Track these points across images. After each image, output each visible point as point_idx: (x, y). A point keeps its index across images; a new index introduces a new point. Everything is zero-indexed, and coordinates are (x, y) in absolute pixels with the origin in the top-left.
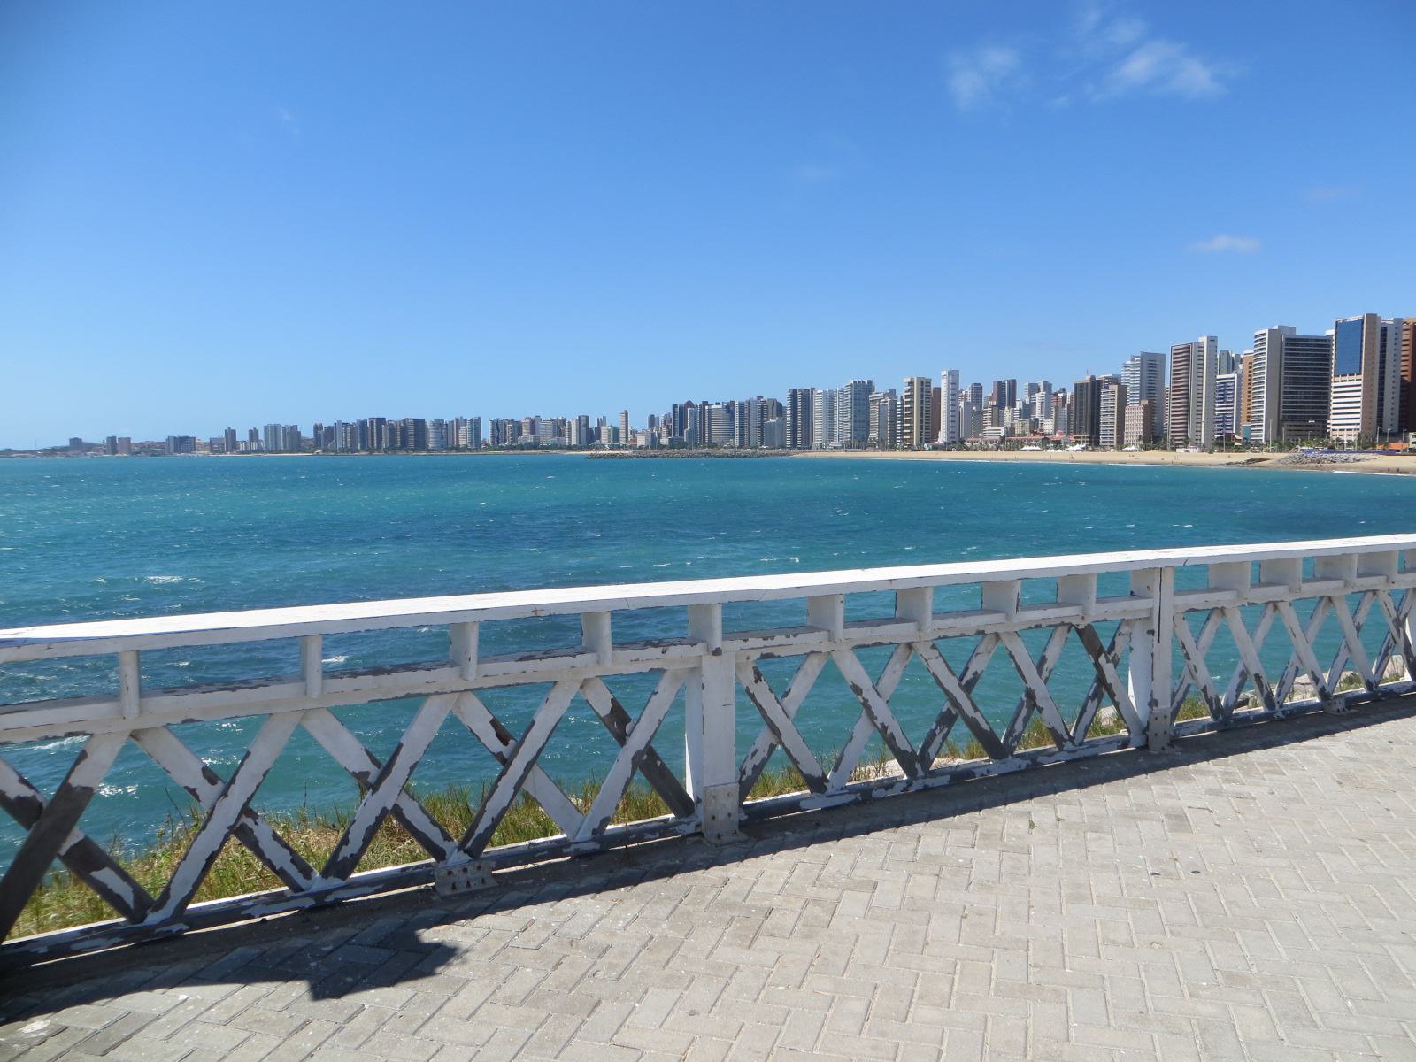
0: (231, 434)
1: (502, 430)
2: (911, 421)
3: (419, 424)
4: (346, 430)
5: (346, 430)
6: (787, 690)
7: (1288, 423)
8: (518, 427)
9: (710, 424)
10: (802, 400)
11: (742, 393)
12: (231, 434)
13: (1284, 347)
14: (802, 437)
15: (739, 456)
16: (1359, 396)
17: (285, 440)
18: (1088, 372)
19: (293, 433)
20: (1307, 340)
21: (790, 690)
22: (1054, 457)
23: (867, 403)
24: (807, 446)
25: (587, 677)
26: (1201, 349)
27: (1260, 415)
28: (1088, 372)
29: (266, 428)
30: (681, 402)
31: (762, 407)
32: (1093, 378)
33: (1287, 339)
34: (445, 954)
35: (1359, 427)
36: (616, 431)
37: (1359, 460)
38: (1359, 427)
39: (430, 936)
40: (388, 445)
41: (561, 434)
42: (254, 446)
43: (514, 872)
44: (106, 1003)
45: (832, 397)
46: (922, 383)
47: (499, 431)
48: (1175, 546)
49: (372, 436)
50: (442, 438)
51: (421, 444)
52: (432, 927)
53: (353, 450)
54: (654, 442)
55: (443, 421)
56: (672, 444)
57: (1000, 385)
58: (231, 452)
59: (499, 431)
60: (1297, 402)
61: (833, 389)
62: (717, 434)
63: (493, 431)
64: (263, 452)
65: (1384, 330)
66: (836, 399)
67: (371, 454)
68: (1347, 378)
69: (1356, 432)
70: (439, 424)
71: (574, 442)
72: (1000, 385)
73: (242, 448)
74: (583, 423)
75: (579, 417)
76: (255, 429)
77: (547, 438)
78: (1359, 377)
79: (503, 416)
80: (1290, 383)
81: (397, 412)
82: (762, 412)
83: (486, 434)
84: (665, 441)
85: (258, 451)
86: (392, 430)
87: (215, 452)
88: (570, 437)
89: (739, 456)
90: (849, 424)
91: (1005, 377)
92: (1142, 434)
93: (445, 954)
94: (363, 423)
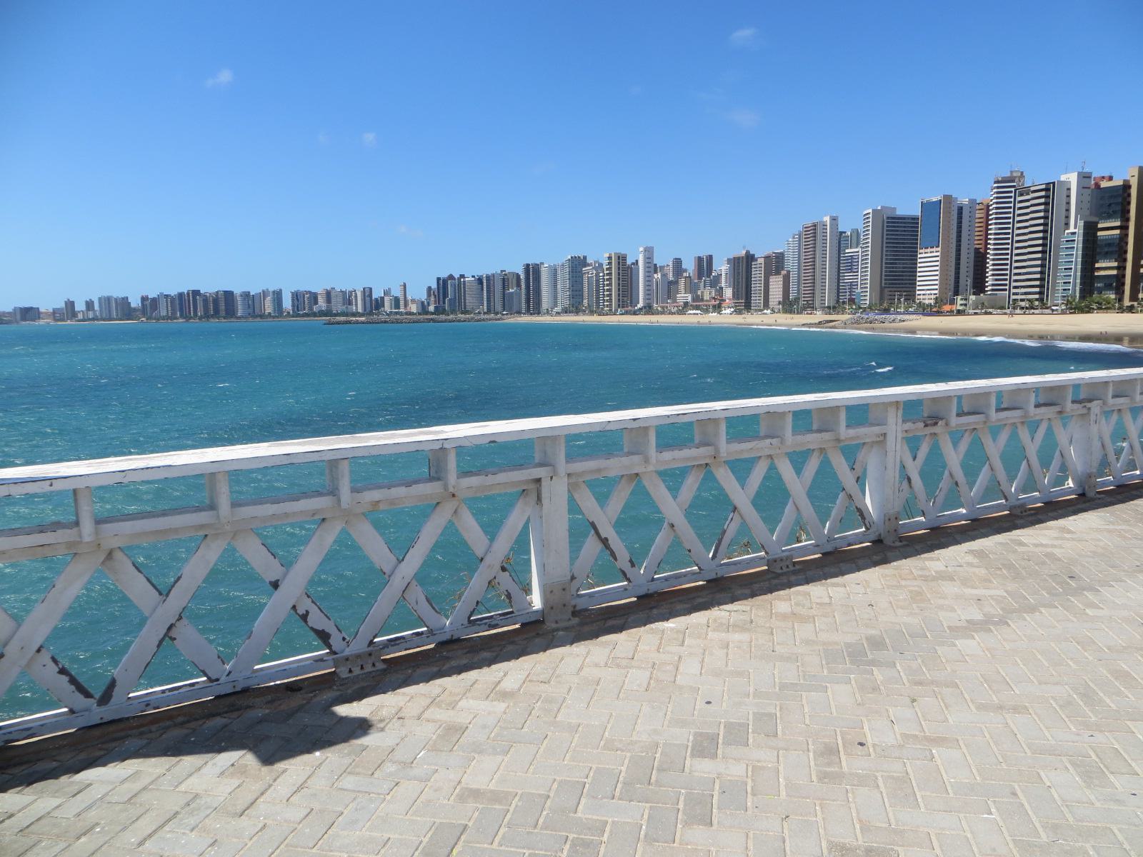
0: (70, 305)
1: (301, 300)
2: (610, 290)
3: (229, 295)
4: (167, 301)
5: (167, 301)
6: (179, 575)
7: (889, 289)
8: (314, 297)
9: (465, 295)
10: (533, 272)
11: (484, 271)
12: (70, 305)
13: (885, 224)
14: (534, 305)
15: (459, 321)
16: (937, 266)
17: (117, 309)
18: (744, 247)
19: (124, 302)
20: (904, 218)
21: (182, 575)
22: (713, 320)
23: (581, 275)
24: (538, 311)
25: (324, 517)
26: (825, 227)
27: (864, 280)
28: (744, 247)
29: (100, 299)
30: (444, 275)
31: (504, 279)
32: (748, 252)
33: (888, 218)
34: (362, 727)
35: (936, 292)
36: (397, 300)
37: (904, 321)
38: (936, 292)
39: (343, 710)
40: (202, 314)
41: (350, 303)
42: (91, 315)
43: (280, 684)
44: (117, 765)
45: (556, 270)
46: (619, 257)
47: (298, 300)
48: (652, 406)
49: (190, 308)
50: (249, 307)
51: (231, 312)
52: (396, 690)
53: (173, 317)
54: (424, 309)
55: (249, 292)
56: (438, 311)
57: (700, 259)
58: (71, 320)
59: (298, 300)
60: (896, 272)
61: (556, 263)
62: (470, 301)
63: (293, 300)
64: (98, 320)
65: (960, 209)
66: (559, 272)
67: (187, 321)
68: (929, 250)
69: (935, 296)
70: (246, 295)
71: (360, 310)
72: (700, 259)
73: (80, 316)
74: (367, 294)
75: (364, 289)
76: (90, 300)
77: (338, 306)
78: (938, 249)
79: (302, 288)
80: (891, 255)
81: (210, 286)
82: (504, 284)
83: (287, 304)
84: (431, 308)
85: (93, 319)
86: (205, 300)
87: (56, 320)
88: (356, 305)
89: (459, 321)
90: (568, 293)
91: (704, 253)
92: (781, 300)
93: (362, 727)
94: (181, 295)
